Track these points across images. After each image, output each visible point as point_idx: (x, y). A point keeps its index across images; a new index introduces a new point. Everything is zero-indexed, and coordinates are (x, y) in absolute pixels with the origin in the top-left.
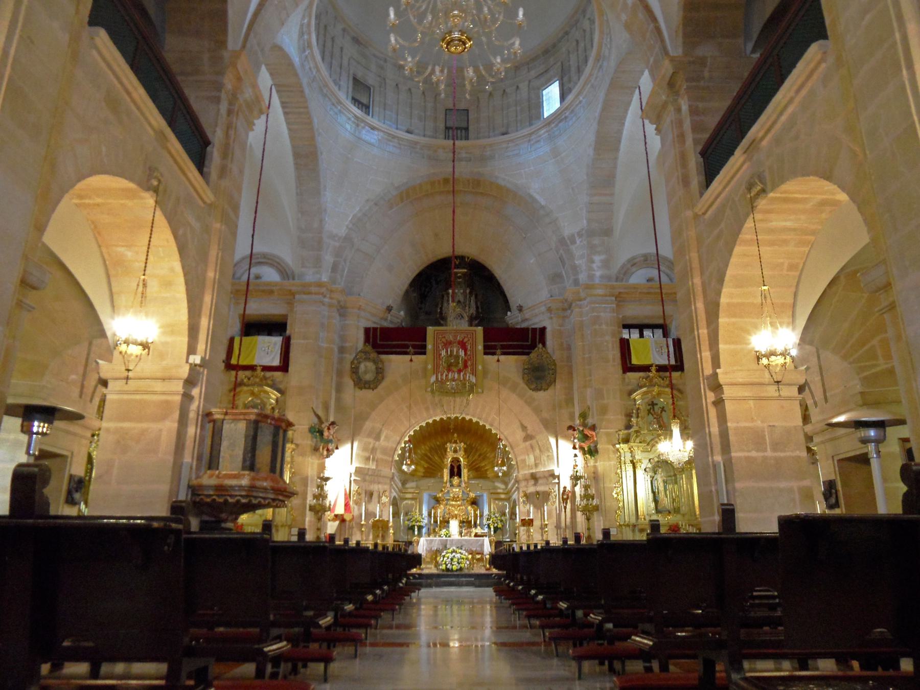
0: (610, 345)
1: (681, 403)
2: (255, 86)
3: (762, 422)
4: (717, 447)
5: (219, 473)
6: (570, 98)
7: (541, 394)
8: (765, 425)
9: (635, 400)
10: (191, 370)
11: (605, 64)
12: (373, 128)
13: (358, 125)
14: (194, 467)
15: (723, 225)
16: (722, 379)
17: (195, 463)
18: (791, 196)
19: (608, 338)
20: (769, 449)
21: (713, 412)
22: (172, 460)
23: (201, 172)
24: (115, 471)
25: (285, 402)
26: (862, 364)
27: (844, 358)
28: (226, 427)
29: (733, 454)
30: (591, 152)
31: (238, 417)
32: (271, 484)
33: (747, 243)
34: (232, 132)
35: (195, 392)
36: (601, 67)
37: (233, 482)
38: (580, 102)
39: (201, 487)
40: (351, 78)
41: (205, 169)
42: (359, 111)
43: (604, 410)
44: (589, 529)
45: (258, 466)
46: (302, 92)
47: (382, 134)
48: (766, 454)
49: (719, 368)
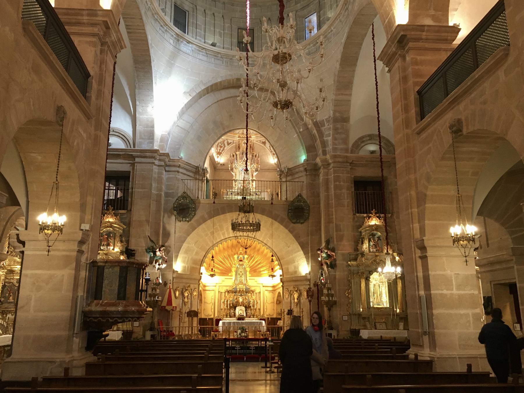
0: (346, 196)
1: (391, 234)
2: (118, 31)
3: (451, 271)
4: (422, 286)
5: (103, 302)
6: (324, 28)
7: (299, 226)
8: (453, 273)
9: (361, 232)
10: (83, 234)
11: (350, 7)
12: (189, 42)
13: (178, 40)
14: (85, 297)
15: (431, 145)
16: (426, 244)
17: (85, 295)
18: (478, 135)
19: (344, 191)
20: (454, 289)
21: (419, 262)
22: (71, 296)
23: (85, 97)
24: (32, 303)
25: (129, 231)
26: (514, 229)
27: (503, 224)
28: (106, 270)
29: (432, 292)
30: (338, 65)
31: (114, 264)
32: (137, 308)
33: (417, 74)
34: (104, 66)
35: (84, 248)
36: (347, 9)
37: (113, 309)
38: (332, 31)
39: (91, 312)
40: (173, 6)
41: (87, 94)
42: (179, 30)
43: (340, 239)
44: (330, 317)
45: (127, 296)
46: (141, 19)
47: (194, 46)
48: (452, 292)
49: (425, 236)
